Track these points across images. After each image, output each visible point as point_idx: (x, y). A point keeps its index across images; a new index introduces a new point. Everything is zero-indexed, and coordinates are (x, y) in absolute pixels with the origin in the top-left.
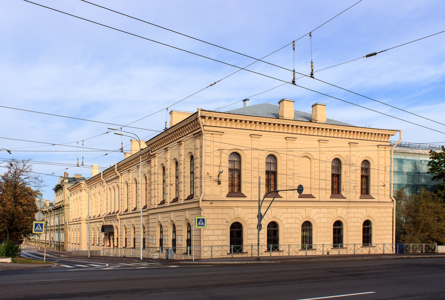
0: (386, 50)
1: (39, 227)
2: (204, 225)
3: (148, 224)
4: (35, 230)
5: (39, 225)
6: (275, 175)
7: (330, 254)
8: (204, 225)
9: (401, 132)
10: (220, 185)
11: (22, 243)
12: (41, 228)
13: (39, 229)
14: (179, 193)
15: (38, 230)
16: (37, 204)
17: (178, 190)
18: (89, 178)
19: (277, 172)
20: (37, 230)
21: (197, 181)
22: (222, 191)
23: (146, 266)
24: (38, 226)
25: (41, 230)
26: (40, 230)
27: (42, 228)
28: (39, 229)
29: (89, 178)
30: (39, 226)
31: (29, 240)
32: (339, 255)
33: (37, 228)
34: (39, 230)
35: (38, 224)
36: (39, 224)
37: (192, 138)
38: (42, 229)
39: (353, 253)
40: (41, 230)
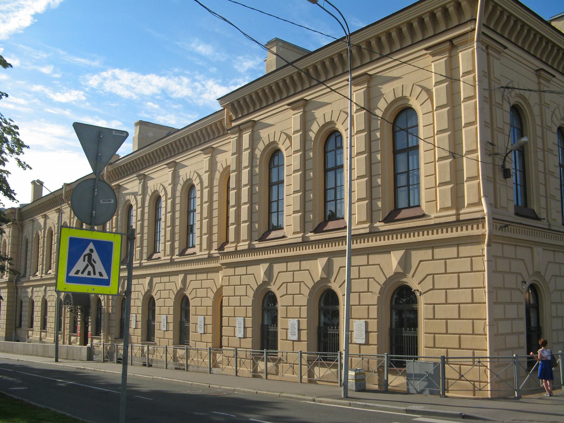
0: (441, 75)
1: (89, 261)
2: (105, 277)
4: (72, 274)
5: (91, 251)
6: (484, 224)
8: (105, 277)
11: (460, 414)
12: (99, 267)
13: (90, 268)
14: (552, 228)
15: (85, 275)
16: (509, 109)
20: (80, 275)
21: (274, 205)
23: (369, 406)
24: (87, 251)
25: (101, 274)
26: (97, 276)
27: (108, 270)
28: (90, 268)
30: (90, 256)
31: (335, 360)
33: (80, 264)
34: (92, 276)
35: (87, 242)
36: (91, 246)
38: (109, 272)
39: (131, 313)
40: (101, 274)
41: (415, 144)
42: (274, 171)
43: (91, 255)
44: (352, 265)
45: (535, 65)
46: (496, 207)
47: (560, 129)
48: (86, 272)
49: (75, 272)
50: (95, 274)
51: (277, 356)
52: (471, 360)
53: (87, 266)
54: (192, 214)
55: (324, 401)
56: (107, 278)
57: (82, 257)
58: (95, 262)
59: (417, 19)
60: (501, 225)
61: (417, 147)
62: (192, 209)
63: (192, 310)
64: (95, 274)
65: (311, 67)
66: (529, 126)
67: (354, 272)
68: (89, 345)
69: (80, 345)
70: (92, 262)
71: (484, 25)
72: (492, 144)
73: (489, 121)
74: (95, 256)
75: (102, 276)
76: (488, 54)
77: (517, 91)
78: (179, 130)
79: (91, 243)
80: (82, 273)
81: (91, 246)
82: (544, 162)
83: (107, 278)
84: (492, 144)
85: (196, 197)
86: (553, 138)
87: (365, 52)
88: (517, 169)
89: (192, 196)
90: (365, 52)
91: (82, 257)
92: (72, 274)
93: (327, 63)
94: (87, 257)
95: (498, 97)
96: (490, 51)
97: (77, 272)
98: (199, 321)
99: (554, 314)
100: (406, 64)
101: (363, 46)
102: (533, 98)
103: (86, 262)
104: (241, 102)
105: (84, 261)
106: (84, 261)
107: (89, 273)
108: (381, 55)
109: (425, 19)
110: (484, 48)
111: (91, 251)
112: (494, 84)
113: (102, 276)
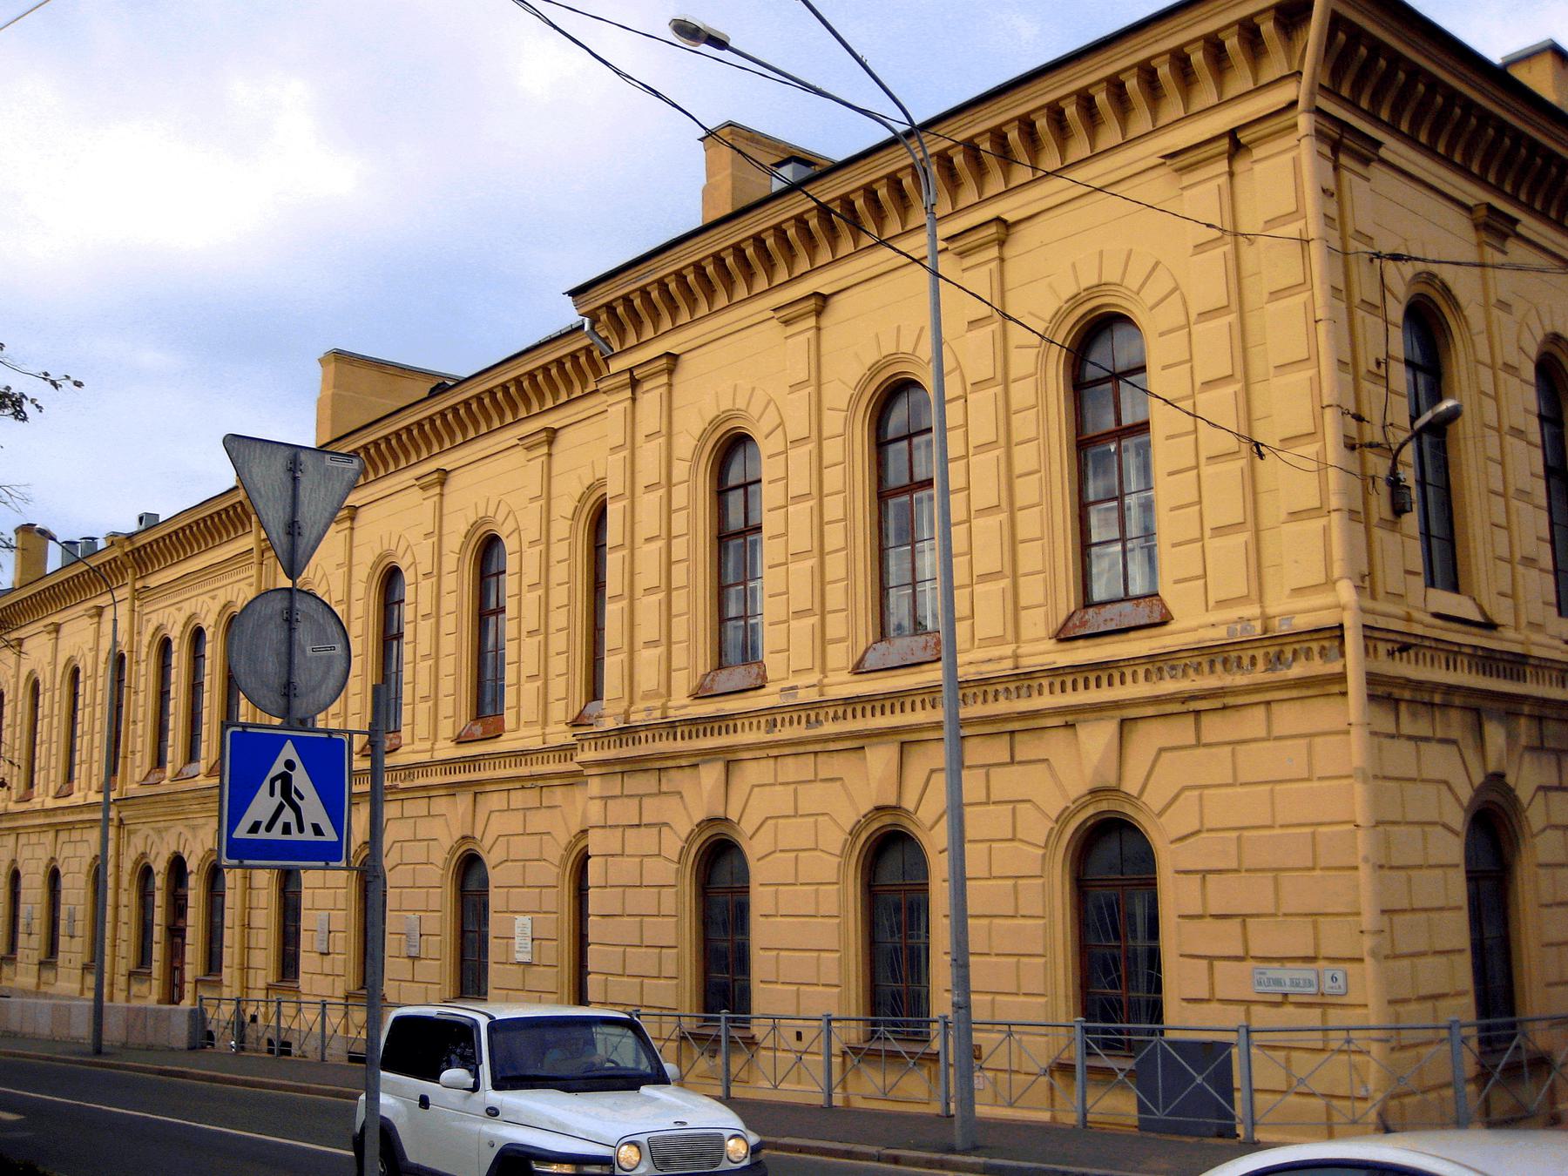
1: (286, 792)
2: (330, 835)
3: (860, 752)
4: (241, 832)
5: (290, 765)
7: (948, 913)
8: (330, 835)
9: (554, 833)
10: (483, 1112)
12: (313, 808)
13: (288, 815)
15: (276, 834)
17: (1190, 739)
18: (922, 329)
19: (1144, 512)
20: (262, 834)
22: (984, 799)
24: (278, 768)
25: (317, 830)
26: (309, 835)
28: (288, 815)
29: (922, 329)
30: (286, 779)
32: (952, 881)
33: (263, 804)
34: (295, 836)
37: (1100, 190)
40: (317, 830)
41: (1140, 419)
42: (735, 500)
43: (290, 776)
44: (966, 764)
45: (1470, 196)
46: (1373, 597)
47: (1546, 368)
48: (279, 825)
49: (248, 828)
50: (301, 829)
51: (177, 866)
52: (1319, 1035)
53: (280, 808)
54: (492, 619)
55: (965, 1163)
56: (334, 838)
57: (266, 784)
58: (301, 798)
59: (1136, 70)
60: (1390, 646)
61: (1143, 427)
62: (493, 605)
63: (495, 899)
64: (301, 829)
65: (838, 202)
66: (1460, 365)
67: (972, 786)
68: (187, 1003)
69: (159, 1002)
70: (294, 796)
71: (1321, 86)
72: (1359, 418)
73: (1341, 286)
74: (301, 779)
75: (322, 834)
76: (1336, 168)
77: (1420, 266)
78: (461, 382)
79: (289, 745)
80: (269, 828)
81: (289, 752)
82: (1502, 463)
83: (334, 838)
84: (1359, 418)
85: (504, 572)
86: (1523, 401)
87: (991, 161)
88: (1432, 533)
89: (494, 570)
90: (991, 161)
91: (266, 784)
92: (241, 832)
93: (883, 193)
94: (278, 784)
95: (1366, 288)
96: (1343, 159)
97: (255, 828)
98: (517, 931)
99: (1547, 899)
100: (1102, 195)
101: (986, 146)
102: (1463, 284)
103: (278, 798)
104: (635, 303)
105: (272, 794)
106: (272, 794)
107: (286, 829)
108: (1035, 168)
109: (1158, 70)
110: (1327, 151)
111: (290, 765)
112: (1363, 317)
113: (322, 834)
